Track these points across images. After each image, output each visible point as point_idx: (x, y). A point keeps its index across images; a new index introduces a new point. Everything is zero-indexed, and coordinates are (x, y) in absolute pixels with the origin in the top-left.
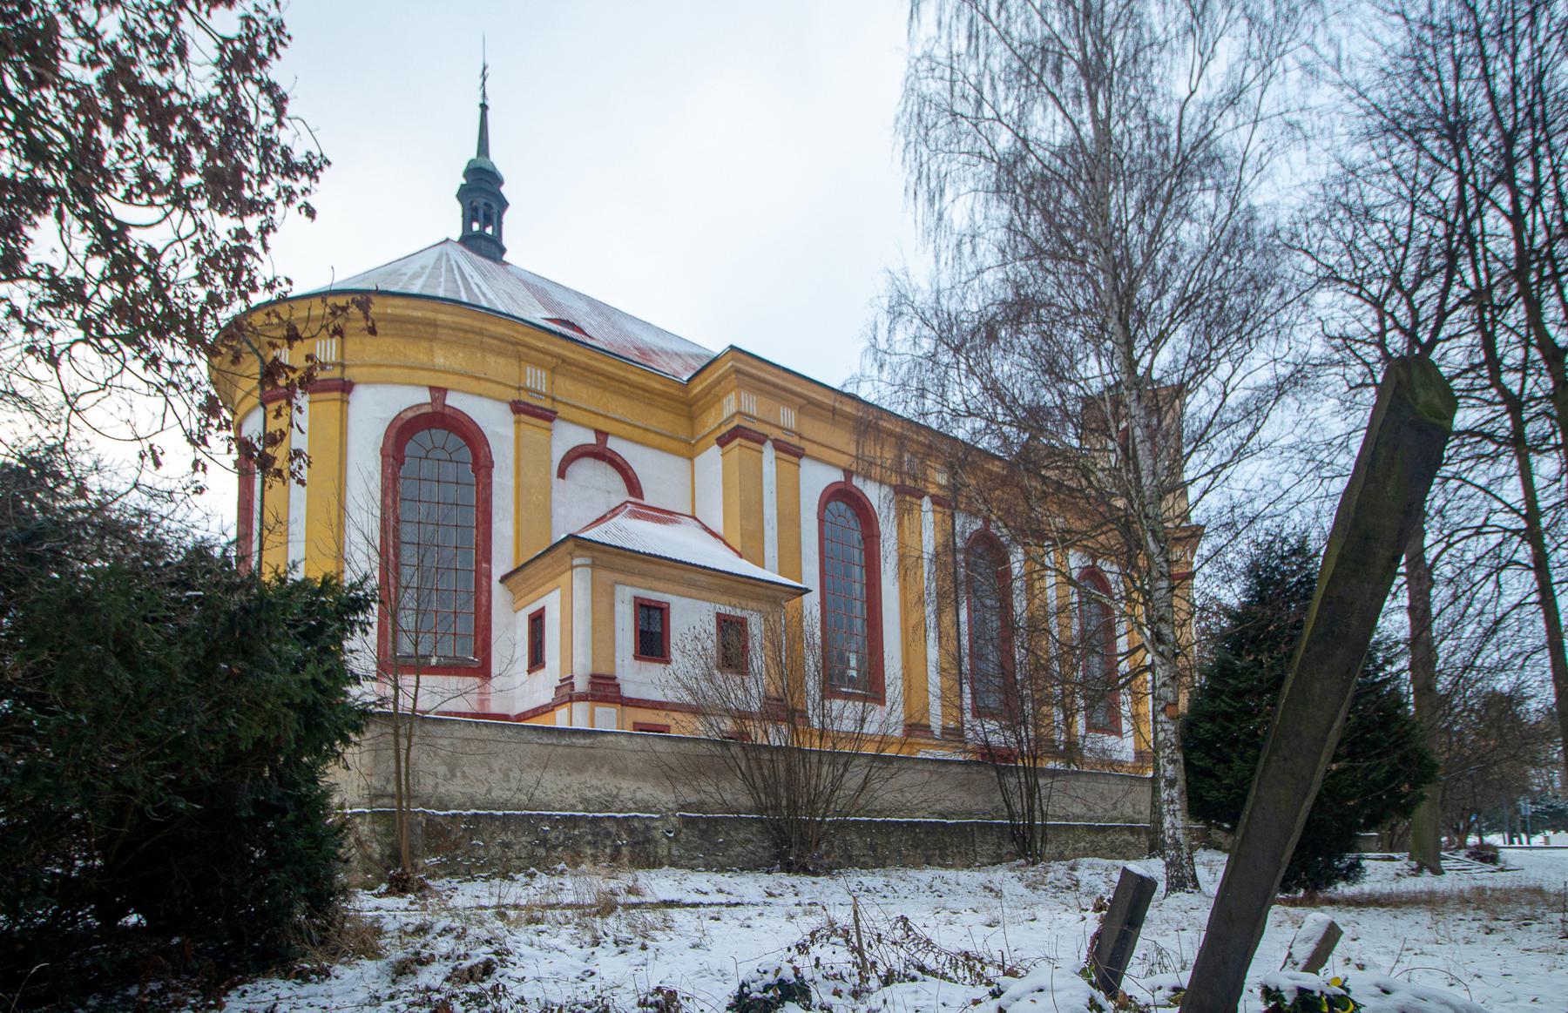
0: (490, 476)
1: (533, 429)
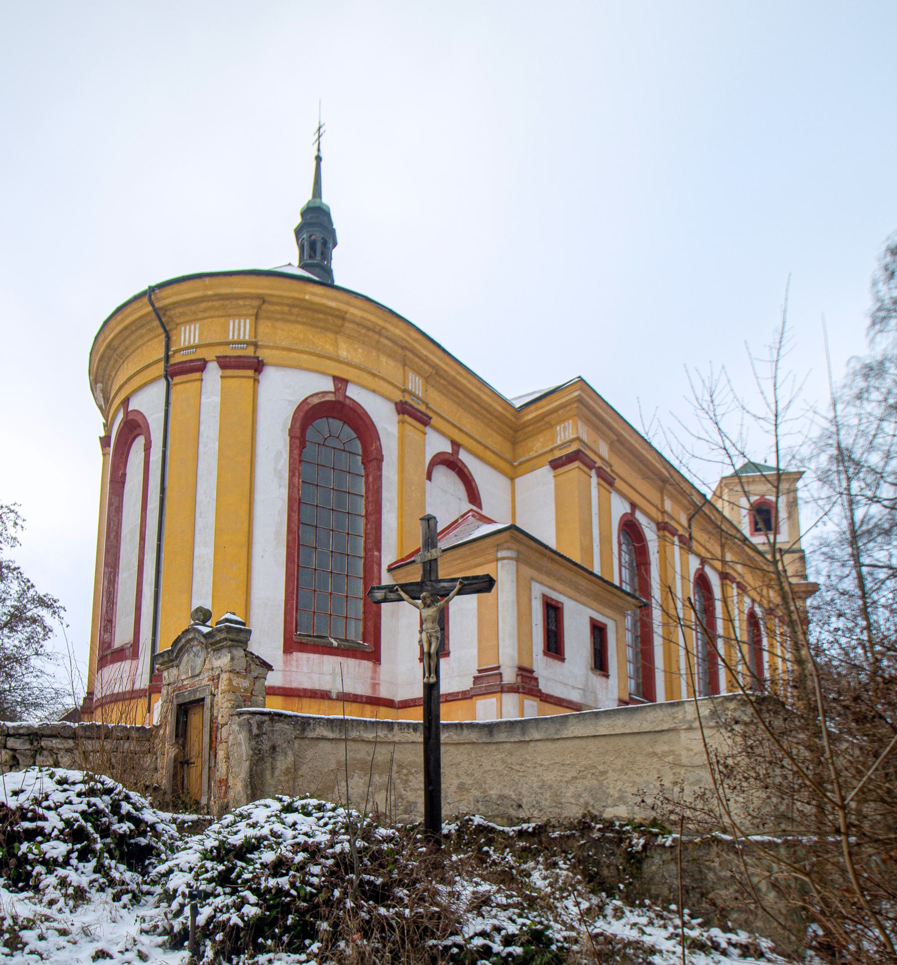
0: (380, 469)
1: (412, 428)
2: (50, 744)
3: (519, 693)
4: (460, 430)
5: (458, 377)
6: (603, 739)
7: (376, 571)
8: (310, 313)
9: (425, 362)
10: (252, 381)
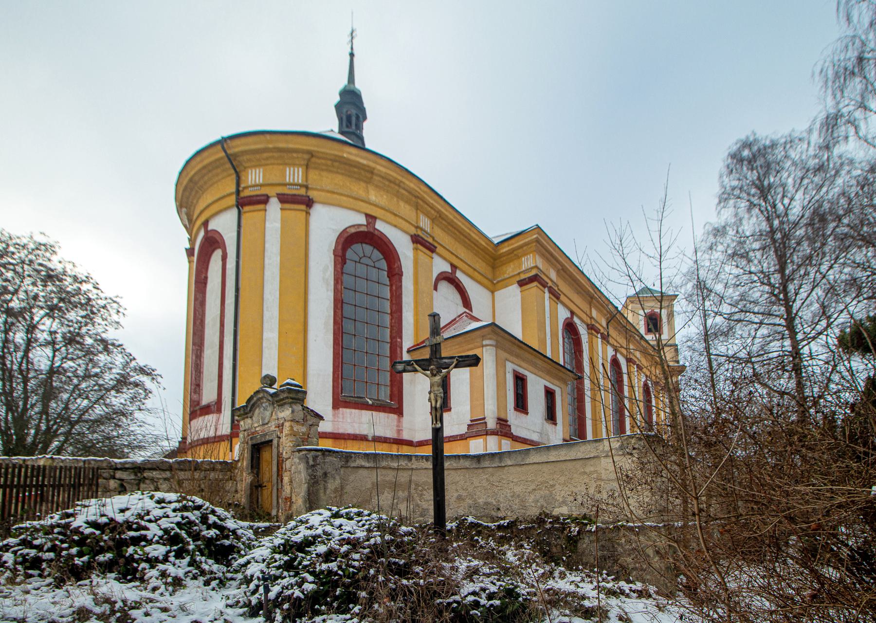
0: (401, 281)
4: (457, 257)
5: (455, 220)
8: (347, 167)
9: (431, 208)
10: (304, 213)
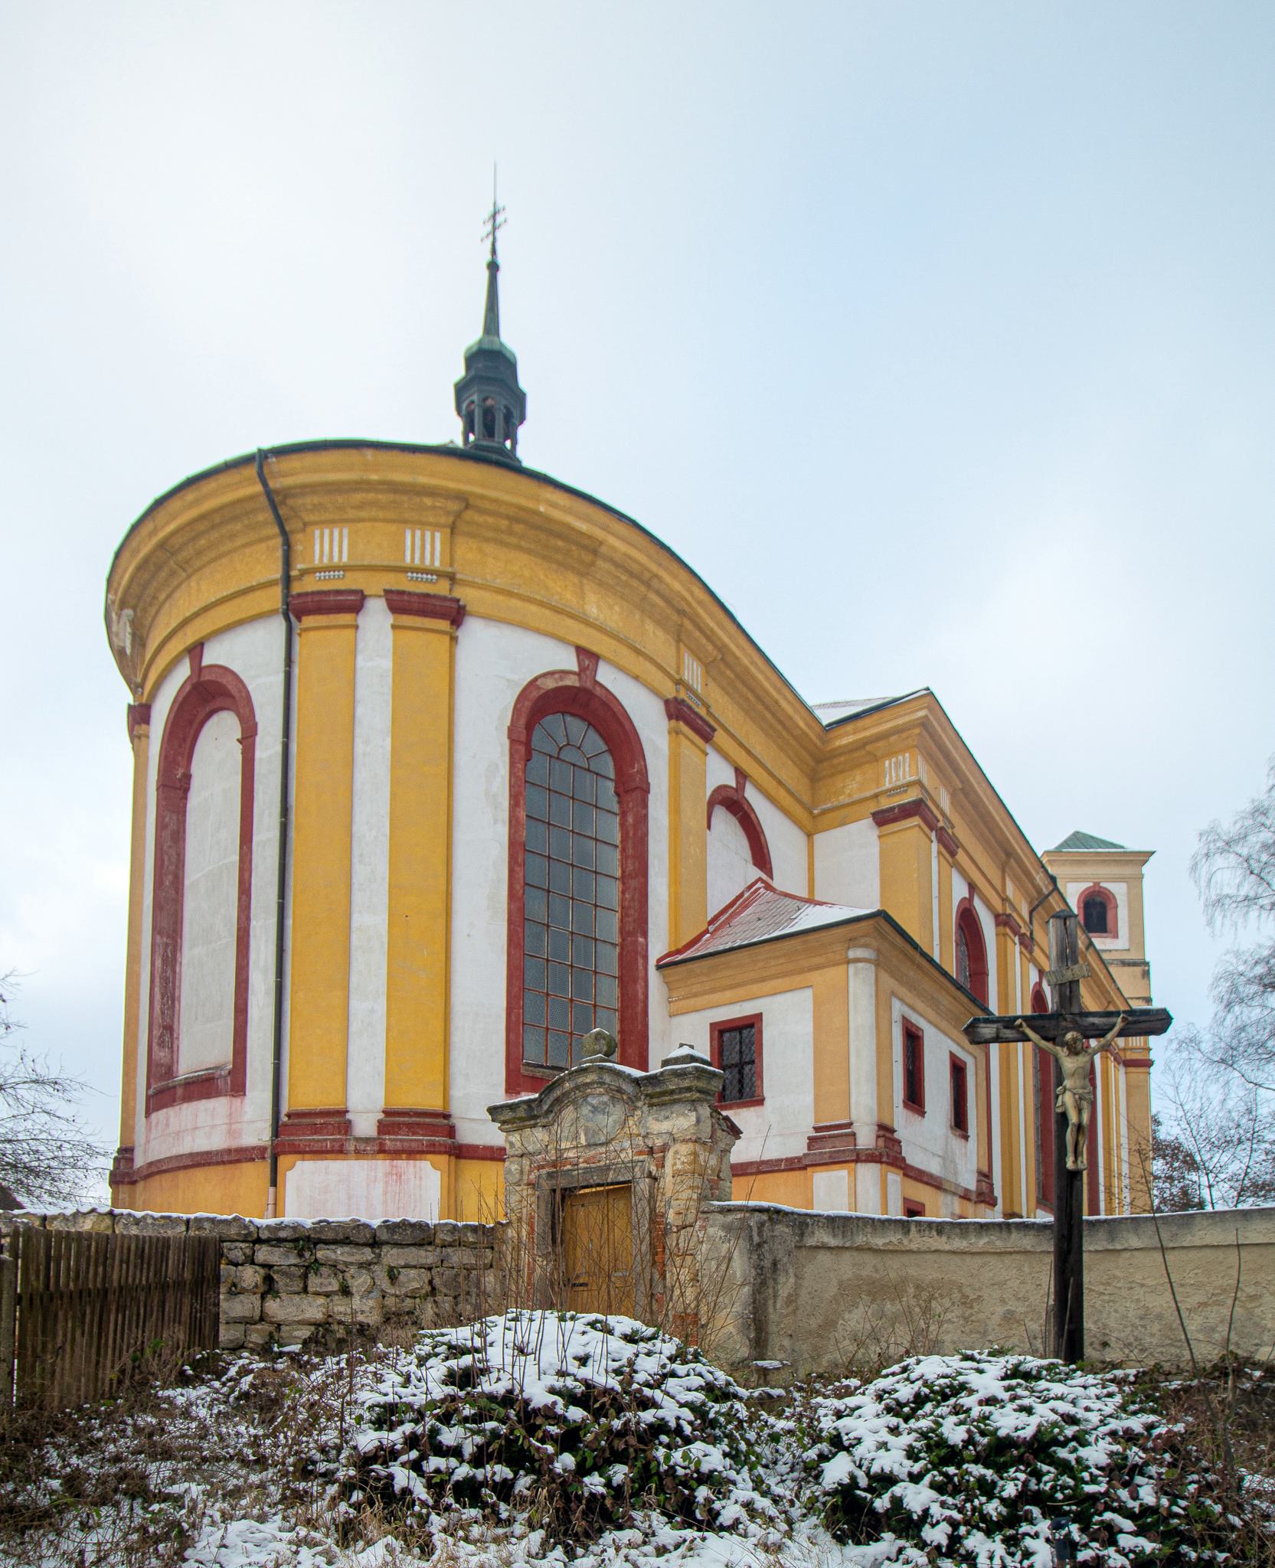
0: (645, 806)
2: (333, 1256)
3: (881, 1162)
4: (749, 752)
5: (753, 669)
6: (1255, 1249)
7: (641, 967)
8: (543, 536)
9: (708, 638)
10: (447, 639)
